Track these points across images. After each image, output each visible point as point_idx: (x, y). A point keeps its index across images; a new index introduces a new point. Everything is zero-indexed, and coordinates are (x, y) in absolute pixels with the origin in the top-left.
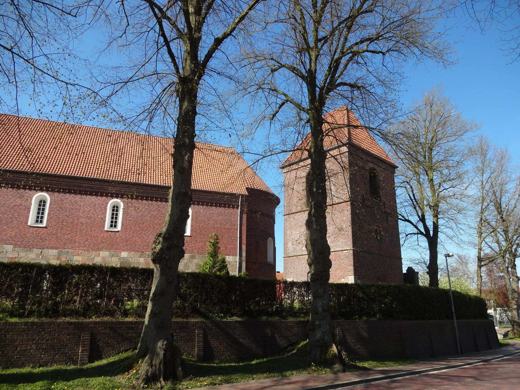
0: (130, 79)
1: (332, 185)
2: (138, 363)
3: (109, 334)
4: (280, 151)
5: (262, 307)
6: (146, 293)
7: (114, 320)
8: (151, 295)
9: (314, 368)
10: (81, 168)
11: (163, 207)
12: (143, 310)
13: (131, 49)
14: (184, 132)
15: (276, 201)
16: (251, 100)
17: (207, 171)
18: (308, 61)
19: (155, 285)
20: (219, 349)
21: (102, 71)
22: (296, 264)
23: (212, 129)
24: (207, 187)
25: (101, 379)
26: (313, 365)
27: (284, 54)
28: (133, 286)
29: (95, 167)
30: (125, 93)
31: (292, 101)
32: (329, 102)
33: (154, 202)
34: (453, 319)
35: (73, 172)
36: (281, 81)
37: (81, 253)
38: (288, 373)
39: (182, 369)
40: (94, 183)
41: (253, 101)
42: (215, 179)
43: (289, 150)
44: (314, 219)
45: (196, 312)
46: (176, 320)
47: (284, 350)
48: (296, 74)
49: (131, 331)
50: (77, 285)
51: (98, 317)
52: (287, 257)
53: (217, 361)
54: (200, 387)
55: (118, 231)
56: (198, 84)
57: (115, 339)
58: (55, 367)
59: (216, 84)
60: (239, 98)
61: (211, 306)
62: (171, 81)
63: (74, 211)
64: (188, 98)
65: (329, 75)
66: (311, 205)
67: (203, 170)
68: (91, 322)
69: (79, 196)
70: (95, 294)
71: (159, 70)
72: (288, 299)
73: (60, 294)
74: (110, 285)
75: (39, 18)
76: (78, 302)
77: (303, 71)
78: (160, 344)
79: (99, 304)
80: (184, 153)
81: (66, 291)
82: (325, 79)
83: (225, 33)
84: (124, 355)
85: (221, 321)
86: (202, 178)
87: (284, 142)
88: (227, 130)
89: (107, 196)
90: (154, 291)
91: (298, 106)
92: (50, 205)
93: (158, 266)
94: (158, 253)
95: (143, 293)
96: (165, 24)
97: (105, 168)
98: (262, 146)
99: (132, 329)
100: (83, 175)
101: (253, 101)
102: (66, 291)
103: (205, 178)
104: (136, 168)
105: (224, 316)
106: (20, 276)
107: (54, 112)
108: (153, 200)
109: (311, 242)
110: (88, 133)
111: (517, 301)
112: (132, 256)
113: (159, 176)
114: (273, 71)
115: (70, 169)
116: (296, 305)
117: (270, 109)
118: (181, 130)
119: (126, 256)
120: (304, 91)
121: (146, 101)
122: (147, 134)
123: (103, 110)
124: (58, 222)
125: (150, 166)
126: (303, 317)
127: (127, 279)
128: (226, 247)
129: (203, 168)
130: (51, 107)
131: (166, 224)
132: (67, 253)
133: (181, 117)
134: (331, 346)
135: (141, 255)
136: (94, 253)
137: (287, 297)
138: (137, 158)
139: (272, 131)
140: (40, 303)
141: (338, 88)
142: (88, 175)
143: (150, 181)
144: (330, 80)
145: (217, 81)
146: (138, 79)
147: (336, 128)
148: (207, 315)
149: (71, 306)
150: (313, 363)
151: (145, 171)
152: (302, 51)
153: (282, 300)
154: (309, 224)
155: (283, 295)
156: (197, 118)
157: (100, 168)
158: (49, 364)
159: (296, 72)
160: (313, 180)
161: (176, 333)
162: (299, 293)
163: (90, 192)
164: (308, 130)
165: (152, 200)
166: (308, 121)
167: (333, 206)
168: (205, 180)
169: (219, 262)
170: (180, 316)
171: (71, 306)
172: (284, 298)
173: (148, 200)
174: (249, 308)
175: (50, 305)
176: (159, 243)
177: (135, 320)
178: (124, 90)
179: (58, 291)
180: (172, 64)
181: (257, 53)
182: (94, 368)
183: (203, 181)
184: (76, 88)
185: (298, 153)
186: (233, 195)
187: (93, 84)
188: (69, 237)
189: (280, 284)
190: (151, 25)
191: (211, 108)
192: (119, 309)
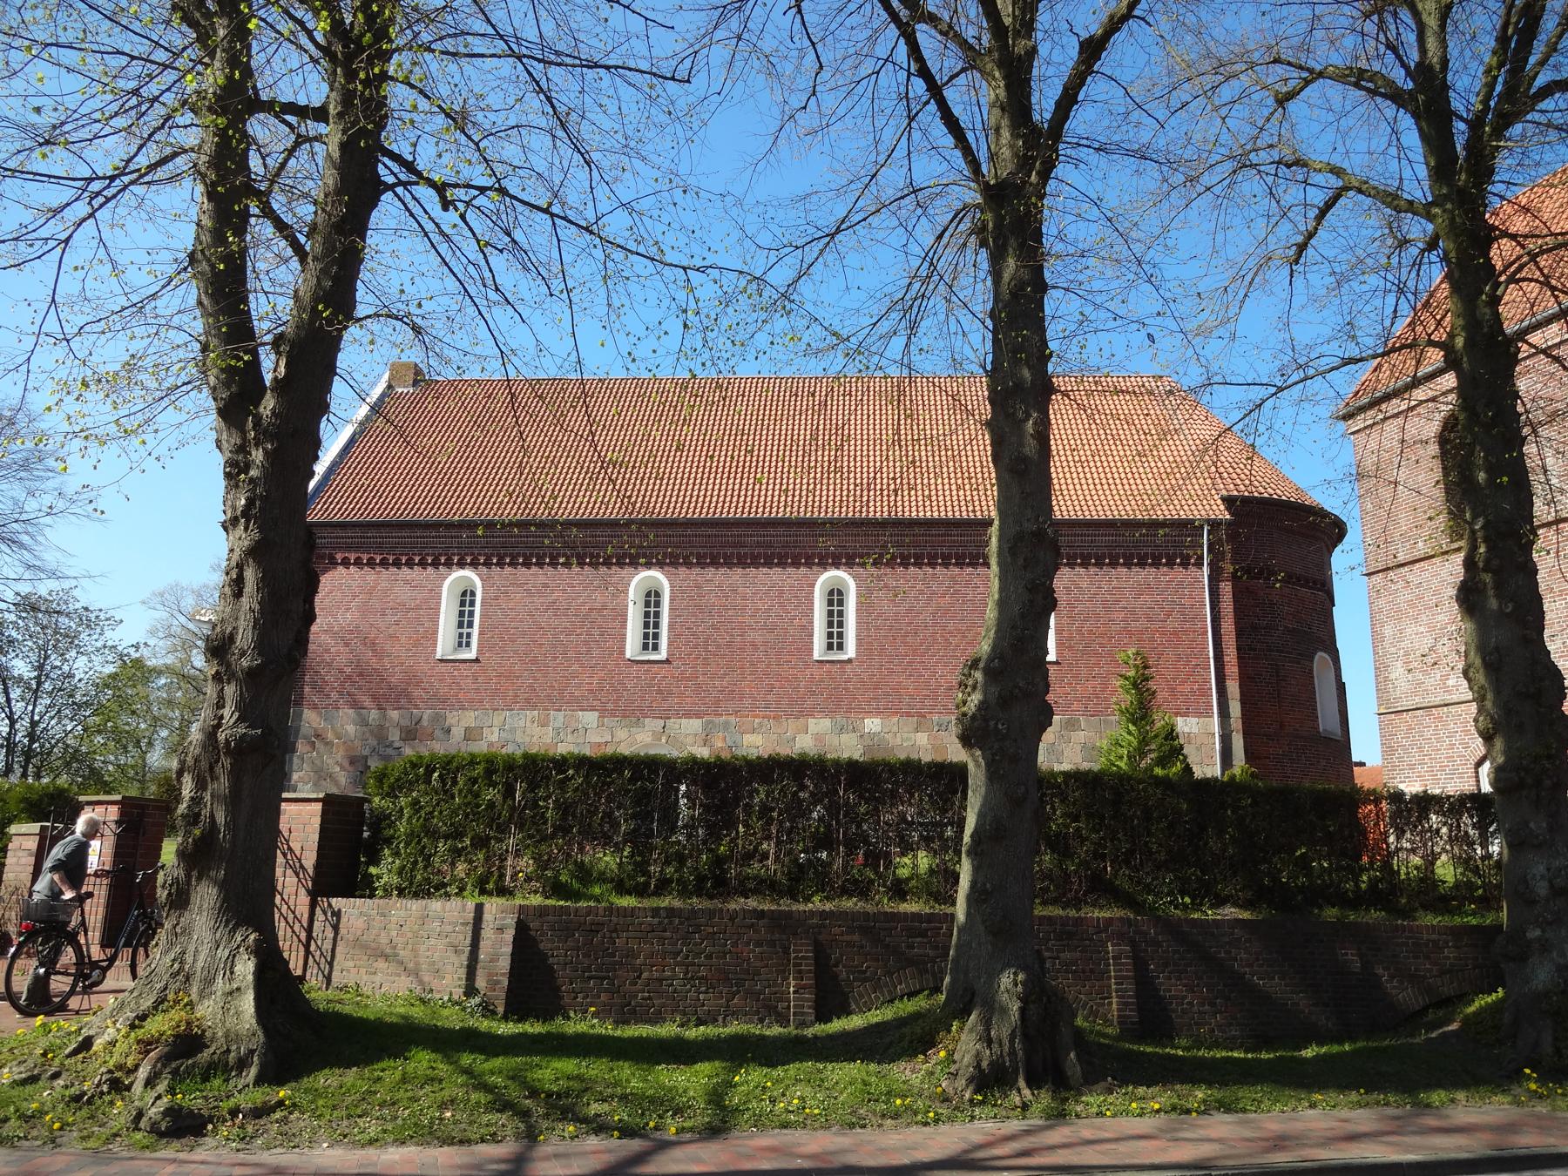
0: (843, 222)
1: (1549, 452)
2: (949, 1031)
3: (862, 947)
4: (1336, 361)
5: (1319, 877)
6: (949, 832)
7: (870, 908)
8: (967, 839)
9: (1533, 1086)
10: (736, 493)
11: (968, 584)
12: (946, 881)
13: (833, 136)
14: (1015, 351)
15: (1334, 530)
16: (1216, 212)
17: (1097, 458)
18: (1410, 38)
19: (976, 810)
20: (1188, 1003)
21: (766, 216)
22: (1427, 734)
23: (1101, 327)
24: (1092, 508)
25: (853, 1070)
26: (1529, 1078)
27: (1319, 34)
28: (911, 813)
29: (777, 487)
30: (831, 265)
31: (1364, 187)
32: (1509, 161)
33: (1191, 568)
35: (716, 507)
36: (1316, 128)
38: (1437, 1097)
39: (1077, 1055)
40: (771, 531)
41: (1223, 212)
42: (1118, 481)
43: (1370, 352)
44: (1487, 578)
45: (1102, 889)
46: (1044, 913)
47: (1414, 1020)
48: (1368, 90)
49: (918, 940)
50: (765, 810)
51: (827, 898)
52: (1390, 712)
53: (1184, 1042)
54: (1140, 1115)
55: (850, 661)
56: (1042, 197)
57: (878, 960)
58: (734, 1028)
59: (1098, 185)
60: (1173, 214)
61: (1147, 874)
62: (956, 202)
64: (1015, 245)
65: (1501, 65)
66: (1473, 532)
67: (1083, 458)
68: (811, 911)
69: (739, 571)
70: (814, 836)
71: (919, 181)
72: (1413, 851)
73: (725, 836)
74: (850, 810)
75: (598, 109)
76: (772, 857)
77: (1398, 75)
78: (1006, 980)
79: (827, 865)
80: (1020, 415)
81: (741, 829)
82: (1486, 84)
83: (1112, 17)
84: (908, 1007)
85: (1186, 919)
86: (1076, 481)
87: (1350, 331)
88: (1146, 321)
89: (809, 564)
90: (973, 826)
91: (1392, 200)
92: (672, 600)
93: (978, 753)
94: (974, 717)
95: (942, 832)
96: (927, 37)
97: (805, 487)
98: (1267, 355)
99: (923, 934)
100: (743, 513)
101: (1223, 212)
102: (741, 829)
103: (1083, 481)
104: (885, 475)
105: (1192, 903)
106: (630, 791)
107: (661, 351)
108: (936, 564)
109: (1484, 660)
110: (743, 396)
112: (895, 729)
113: (954, 493)
114: (1283, 100)
115: (708, 499)
116: (1446, 871)
117: (1285, 228)
118: (1006, 345)
119: (878, 729)
120: (1405, 141)
121: (892, 278)
122: (905, 373)
123: (780, 323)
124: (696, 646)
125: (924, 464)
126: (1474, 913)
127: (894, 795)
128: (1173, 690)
129: (1082, 453)
130: (652, 342)
131: (988, 630)
132: (726, 725)
133: (1000, 305)
136: (792, 725)
137: (1408, 845)
138: (884, 448)
139: (1299, 300)
140: (681, 859)
141: (1542, 106)
142: (757, 513)
143: (921, 509)
144: (1505, 82)
145: (1098, 174)
146: (864, 220)
147: (1550, 250)
148: (1140, 898)
149: (755, 868)
150: (1527, 1071)
151: (912, 482)
152: (1382, 8)
153: (1390, 855)
154: (1469, 597)
155: (1392, 839)
156: (1051, 302)
157: (791, 487)
158: (720, 1018)
159: (1370, 85)
160: (1472, 445)
161: (1048, 949)
162: (1450, 831)
163: (766, 556)
164: (1436, 273)
165: (932, 565)
166: (1432, 245)
167: (1561, 526)
168: (1085, 487)
169: (1156, 736)
170: (1055, 902)
171: (755, 868)
172: (1398, 850)
173: (923, 564)
174: (1276, 880)
175: (705, 864)
176: (974, 688)
177: (927, 911)
178: (830, 257)
179: (722, 829)
180: (958, 153)
181: (1223, 53)
182: (832, 1037)
183: (1079, 492)
184: (711, 277)
185: (1404, 364)
186: (1186, 527)
187: (748, 257)
188: (725, 684)
189: (1377, 802)
190: (882, 51)
191: (1092, 262)
192: (880, 878)
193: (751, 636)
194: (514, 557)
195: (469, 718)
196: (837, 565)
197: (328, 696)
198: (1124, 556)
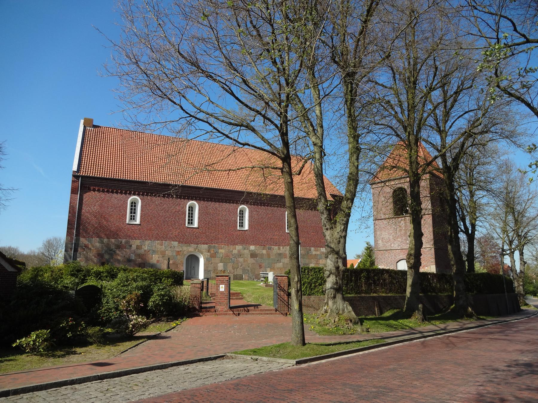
34: (505, 293)
37: (224, 247)
55: (247, 230)
63: (215, 215)
69: (218, 203)
89: (237, 203)
110: (104, 133)
111: (523, 279)
119: (254, 249)
132: (214, 247)
134: (468, 308)
135: (264, 248)
136: (231, 247)
188: (214, 235)
197: (89, 234)
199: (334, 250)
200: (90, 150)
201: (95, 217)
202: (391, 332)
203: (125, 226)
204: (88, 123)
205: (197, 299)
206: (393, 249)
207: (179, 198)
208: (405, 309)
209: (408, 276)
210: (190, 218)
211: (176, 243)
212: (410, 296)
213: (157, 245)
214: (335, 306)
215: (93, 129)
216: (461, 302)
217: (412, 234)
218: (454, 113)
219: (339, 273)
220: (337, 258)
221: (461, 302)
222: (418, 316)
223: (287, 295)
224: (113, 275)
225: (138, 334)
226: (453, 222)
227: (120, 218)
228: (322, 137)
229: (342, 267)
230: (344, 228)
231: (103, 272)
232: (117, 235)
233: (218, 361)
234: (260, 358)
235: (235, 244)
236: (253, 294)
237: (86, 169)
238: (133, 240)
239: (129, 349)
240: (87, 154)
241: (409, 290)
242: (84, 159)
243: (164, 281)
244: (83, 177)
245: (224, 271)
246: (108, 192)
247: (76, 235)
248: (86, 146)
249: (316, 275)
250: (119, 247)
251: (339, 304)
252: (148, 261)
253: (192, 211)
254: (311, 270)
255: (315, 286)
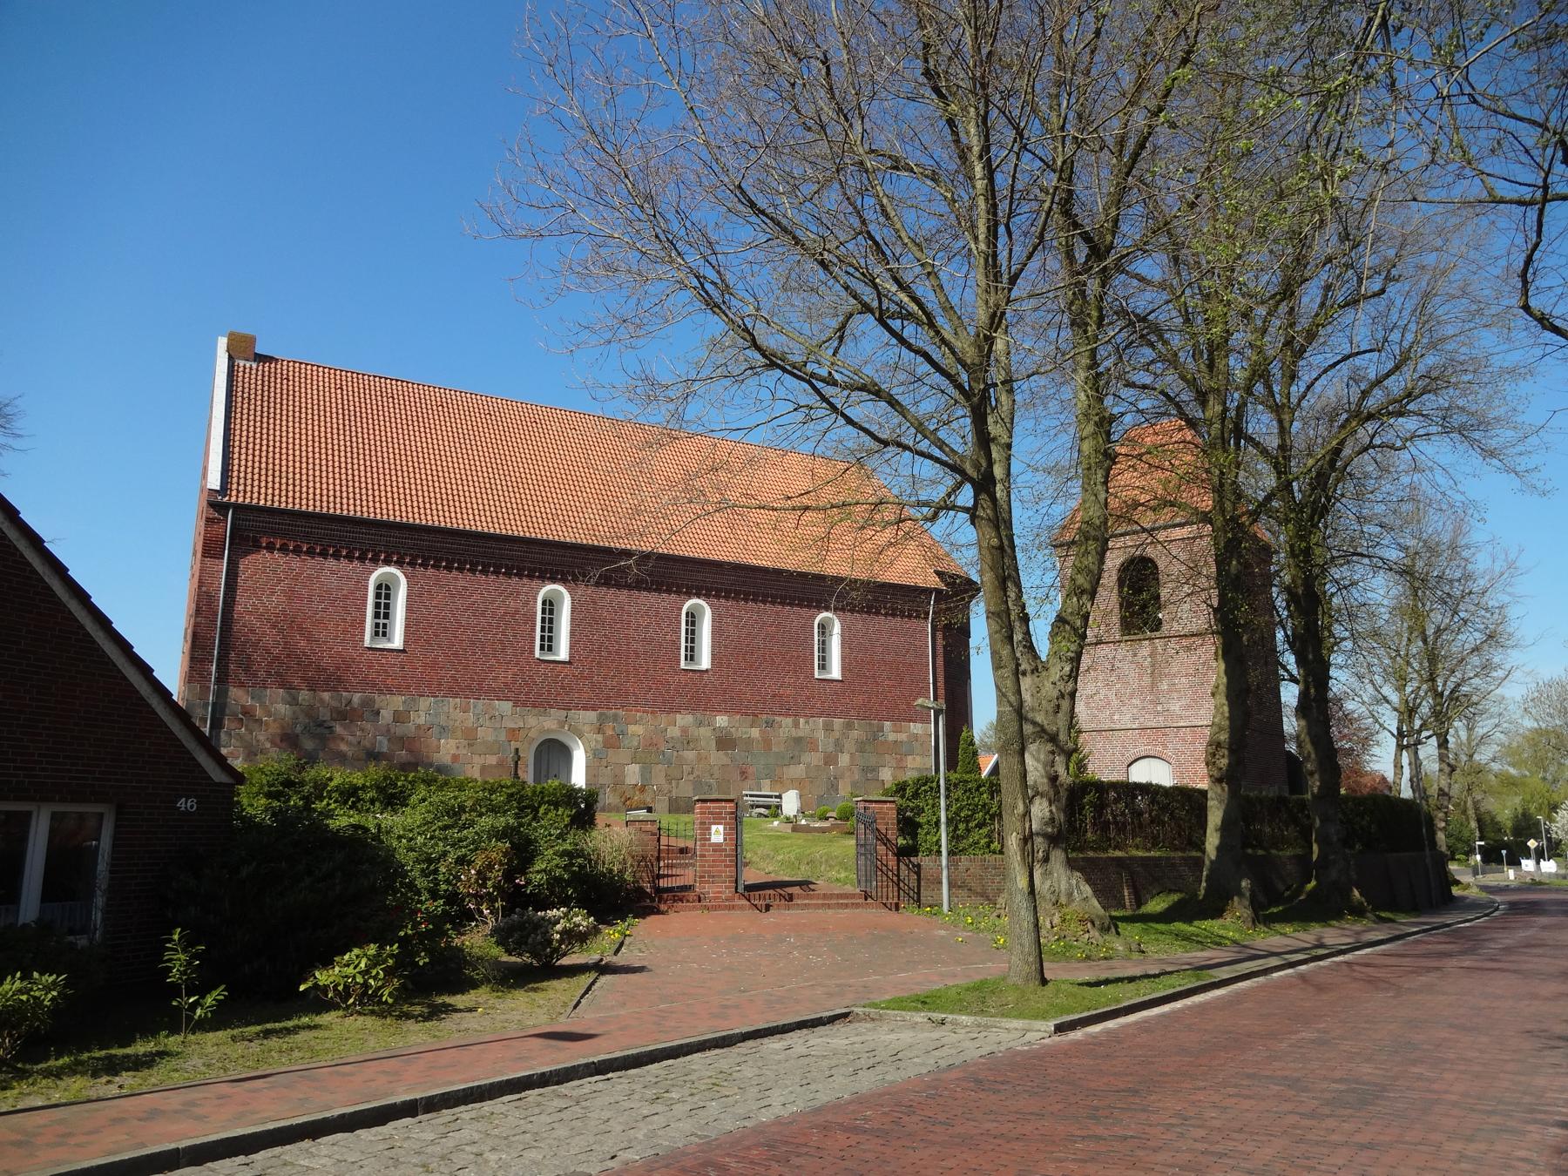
33: (454, 572)
42: (444, 496)
55: (707, 671)
89: (678, 592)
134: (1352, 891)
135: (753, 721)
136: (663, 719)
165: (764, 602)
193: (635, 646)
194: (438, 561)
195: (397, 702)
196: (698, 596)
197: (255, 676)
198: (507, 567)
199: (1043, 730)
200: (251, 429)
201: (274, 627)
202: (1206, 954)
203: (361, 655)
204: (241, 348)
205: (646, 866)
206: (1118, 727)
207: (516, 575)
208: (1203, 892)
209: (1210, 803)
210: (546, 634)
211: (506, 707)
212: (1217, 856)
213: (453, 710)
214: (1048, 883)
215: (254, 366)
216: (1334, 874)
217: (1222, 688)
218: (1316, 359)
219: (1057, 793)
220: (1053, 753)
221: (1334, 874)
222: (1240, 909)
223: (894, 854)
224: (393, 796)
225: (565, 961)
226: (1311, 657)
227: (345, 631)
228: (1012, 419)
229: (1065, 778)
230: (1071, 671)
231: (364, 788)
232: (339, 680)
233: (838, 1026)
234: (950, 1017)
235: (674, 710)
236: (776, 850)
237: (245, 485)
238: (383, 697)
239: (582, 997)
240: (244, 439)
241: (1212, 841)
242: (236, 456)
243: (546, 814)
244: (238, 508)
245: (644, 786)
246: (311, 553)
247: (219, 680)
248: (238, 415)
249: (968, 798)
250: (345, 715)
251: (1059, 877)
252: (428, 757)
253: (551, 612)
254: (956, 786)
255: (968, 830)
